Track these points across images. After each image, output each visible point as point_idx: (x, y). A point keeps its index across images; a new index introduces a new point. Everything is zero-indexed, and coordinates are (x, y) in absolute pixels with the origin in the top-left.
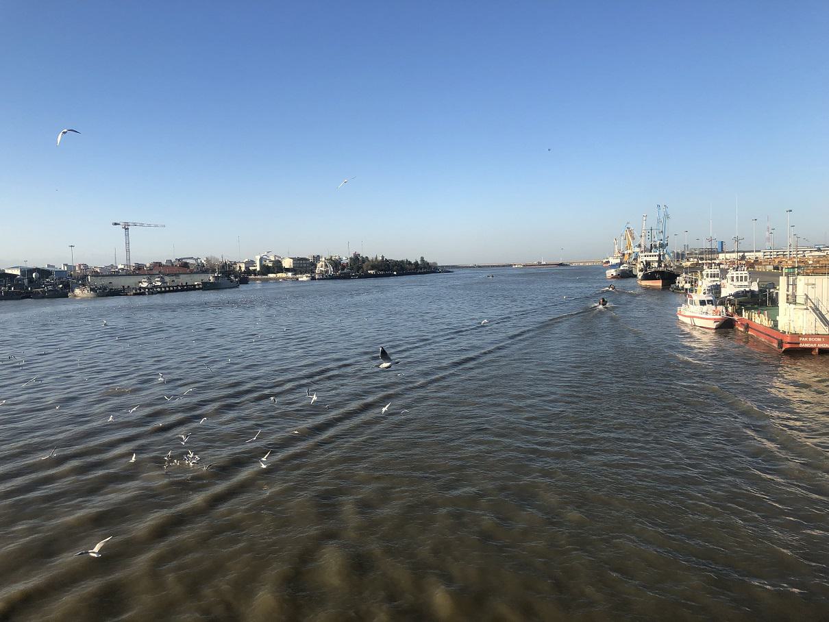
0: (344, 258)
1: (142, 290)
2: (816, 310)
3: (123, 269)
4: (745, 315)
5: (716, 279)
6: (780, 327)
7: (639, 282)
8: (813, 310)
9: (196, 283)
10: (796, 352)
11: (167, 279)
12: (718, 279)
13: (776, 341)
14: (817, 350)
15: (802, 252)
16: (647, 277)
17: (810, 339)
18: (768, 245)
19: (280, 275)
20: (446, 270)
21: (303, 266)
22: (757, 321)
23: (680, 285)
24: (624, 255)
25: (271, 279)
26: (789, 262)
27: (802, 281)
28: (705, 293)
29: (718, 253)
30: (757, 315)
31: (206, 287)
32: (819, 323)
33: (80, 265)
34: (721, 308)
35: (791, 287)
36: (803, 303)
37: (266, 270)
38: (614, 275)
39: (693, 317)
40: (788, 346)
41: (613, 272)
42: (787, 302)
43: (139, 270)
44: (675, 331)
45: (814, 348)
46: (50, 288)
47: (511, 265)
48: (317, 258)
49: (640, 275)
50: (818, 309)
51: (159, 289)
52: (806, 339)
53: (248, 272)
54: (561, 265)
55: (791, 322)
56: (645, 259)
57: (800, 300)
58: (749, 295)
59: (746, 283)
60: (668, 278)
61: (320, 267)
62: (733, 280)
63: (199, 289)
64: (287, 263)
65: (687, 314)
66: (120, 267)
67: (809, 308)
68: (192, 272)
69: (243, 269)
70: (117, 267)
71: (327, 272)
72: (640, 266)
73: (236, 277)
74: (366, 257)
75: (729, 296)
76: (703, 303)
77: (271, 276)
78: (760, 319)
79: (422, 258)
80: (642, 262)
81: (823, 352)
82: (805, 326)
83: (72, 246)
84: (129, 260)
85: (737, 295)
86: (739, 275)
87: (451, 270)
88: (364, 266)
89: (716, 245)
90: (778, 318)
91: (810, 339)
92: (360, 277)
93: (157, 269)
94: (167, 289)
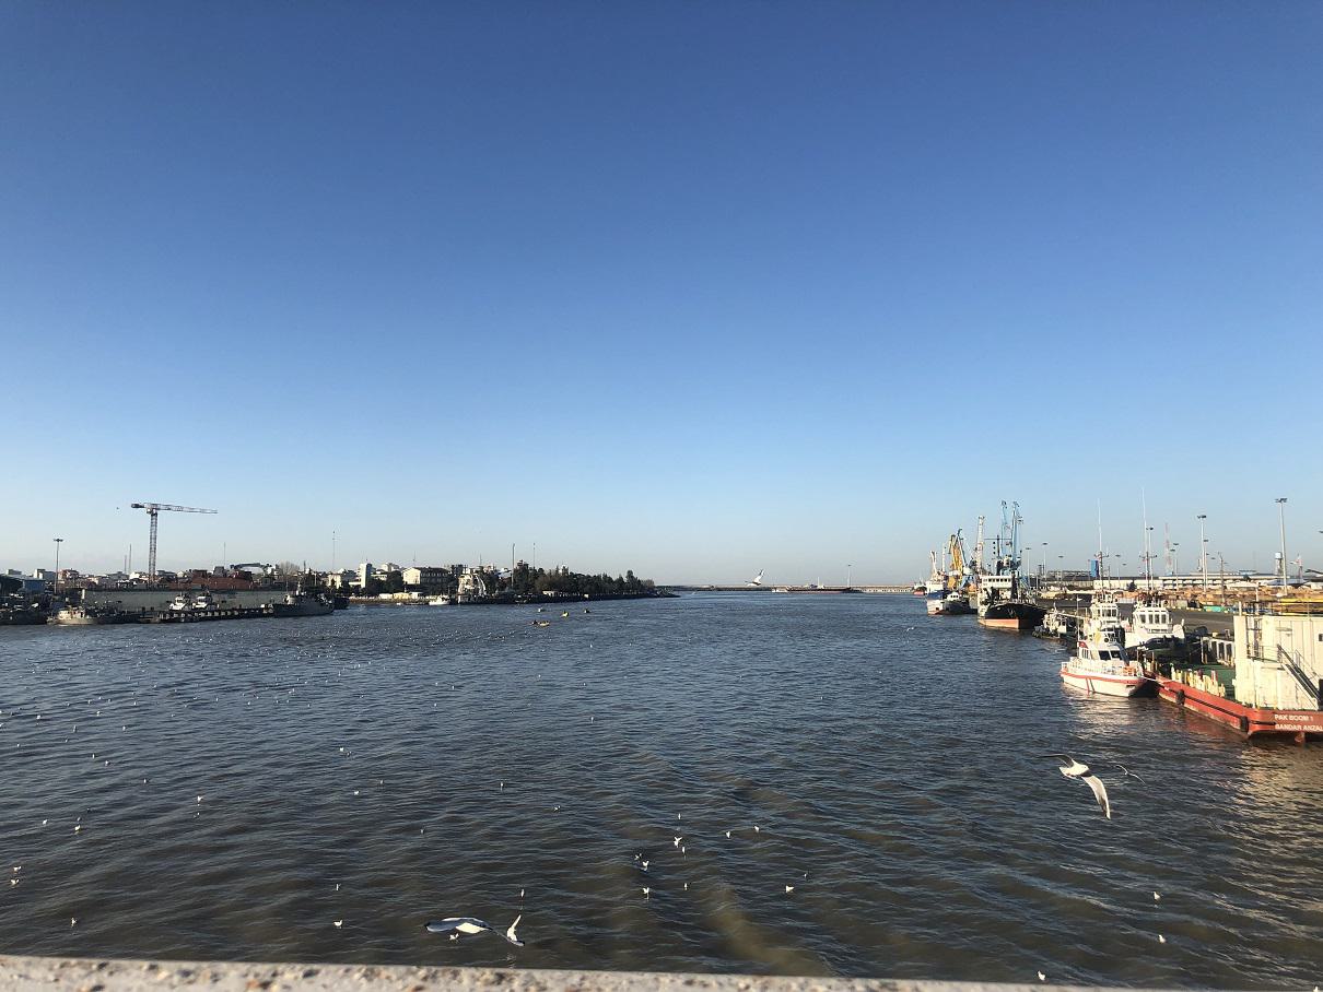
0: (502, 570)
1: (175, 616)
2: (1296, 671)
3: (138, 580)
4: (1176, 676)
5: (1112, 619)
6: (1240, 696)
7: (982, 621)
8: (1291, 669)
9: (263, 606)
10: (1270, 738)
11: (215, 598)
12: (1115, 619)
13: (1237, 720)
14: (1303, 736)
15: (1220, 582)
16: (992, 614)
17: (1292, 718)
18: (1169, 569)
19: (398, 595)
20: (667, 592)
21: (438, 580)
22: (1198, 687)
23: (1052, 628)
24: (947, 578)
25: (383, 601)
26: (1208, 596)
27: (1269, 624)
28: (1106, 640)
29: (1093, 579)
30: (1197, 677)
31: (281, 611)
32: (1302, 692)
33: (65, 571)
34: (1134, 664)
35: (1251, 633)
36: (1275, 658)
37: (375, 586)
38: (941, 608)
39: (1091, 678)
40: (1257, 728)
41: (935, 605)
42: (1249, 657)
43: (167, 582)
44: (1057, 700)
45: (1299, 732)
46: (18, 608)
47: (769, 589)
48: (459, 569)
49: (983, 609)
50: (1298, 670)
51: (202, 615)
52: (1285, 717)
53: (346, 589)
54: (848, 590)
55: (1257, 689)
56: (990, 585)
57: (1270, 653)
58: (1172, 644)
59: (1165, 626)
60: (1031, 617)
61: (465, 583)
62: (1144, 621)
63: (268, 615)
64: (411, 577)
65: (1079, 673)
66: (133, 576)
67: (1285, 667)
68: (256, 588)
69: (338, 584)
70: (128, 577)
71: (476, 591)
72: (983, 596)
73: (328, 598)
74: (519, 564)
75: (1141, 646)
76: (1104, 655)
77: (384, 596)
78: (1204, 685)
79: (630, 573)
80: (985, 589)
81: (1311, 738)
82: (1279, 696)
83: (58, 540)
84: (152, 564)
85: (1152, 644)
86: (1154, 614)
87: (675, 593)
88: (537, 583)
89: (1087, 568)
90: (1234, 682)
91: (1292, 718)
92: (532, 601)
93: (198, 581)
94: (216, 614)
